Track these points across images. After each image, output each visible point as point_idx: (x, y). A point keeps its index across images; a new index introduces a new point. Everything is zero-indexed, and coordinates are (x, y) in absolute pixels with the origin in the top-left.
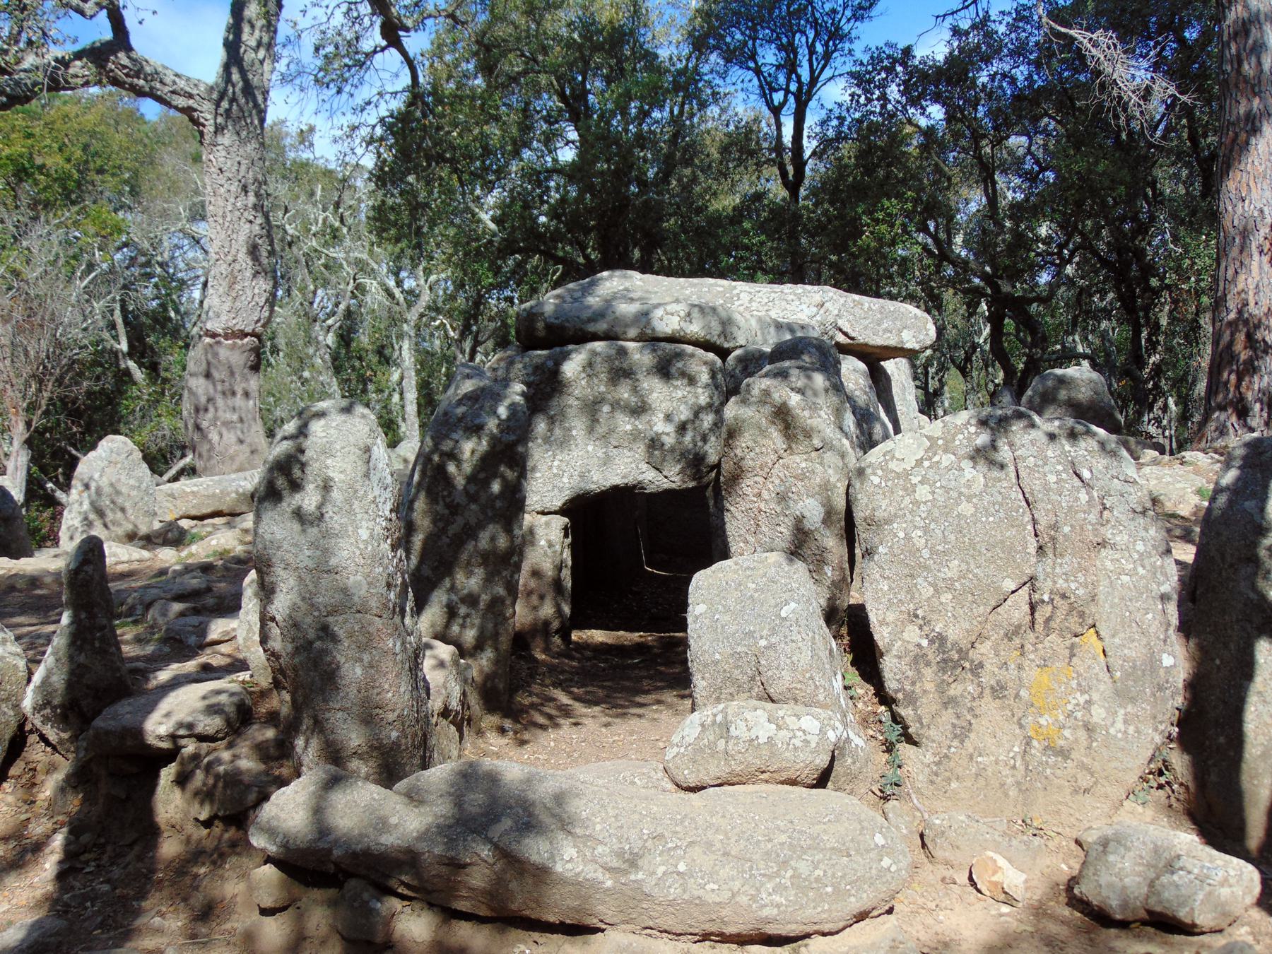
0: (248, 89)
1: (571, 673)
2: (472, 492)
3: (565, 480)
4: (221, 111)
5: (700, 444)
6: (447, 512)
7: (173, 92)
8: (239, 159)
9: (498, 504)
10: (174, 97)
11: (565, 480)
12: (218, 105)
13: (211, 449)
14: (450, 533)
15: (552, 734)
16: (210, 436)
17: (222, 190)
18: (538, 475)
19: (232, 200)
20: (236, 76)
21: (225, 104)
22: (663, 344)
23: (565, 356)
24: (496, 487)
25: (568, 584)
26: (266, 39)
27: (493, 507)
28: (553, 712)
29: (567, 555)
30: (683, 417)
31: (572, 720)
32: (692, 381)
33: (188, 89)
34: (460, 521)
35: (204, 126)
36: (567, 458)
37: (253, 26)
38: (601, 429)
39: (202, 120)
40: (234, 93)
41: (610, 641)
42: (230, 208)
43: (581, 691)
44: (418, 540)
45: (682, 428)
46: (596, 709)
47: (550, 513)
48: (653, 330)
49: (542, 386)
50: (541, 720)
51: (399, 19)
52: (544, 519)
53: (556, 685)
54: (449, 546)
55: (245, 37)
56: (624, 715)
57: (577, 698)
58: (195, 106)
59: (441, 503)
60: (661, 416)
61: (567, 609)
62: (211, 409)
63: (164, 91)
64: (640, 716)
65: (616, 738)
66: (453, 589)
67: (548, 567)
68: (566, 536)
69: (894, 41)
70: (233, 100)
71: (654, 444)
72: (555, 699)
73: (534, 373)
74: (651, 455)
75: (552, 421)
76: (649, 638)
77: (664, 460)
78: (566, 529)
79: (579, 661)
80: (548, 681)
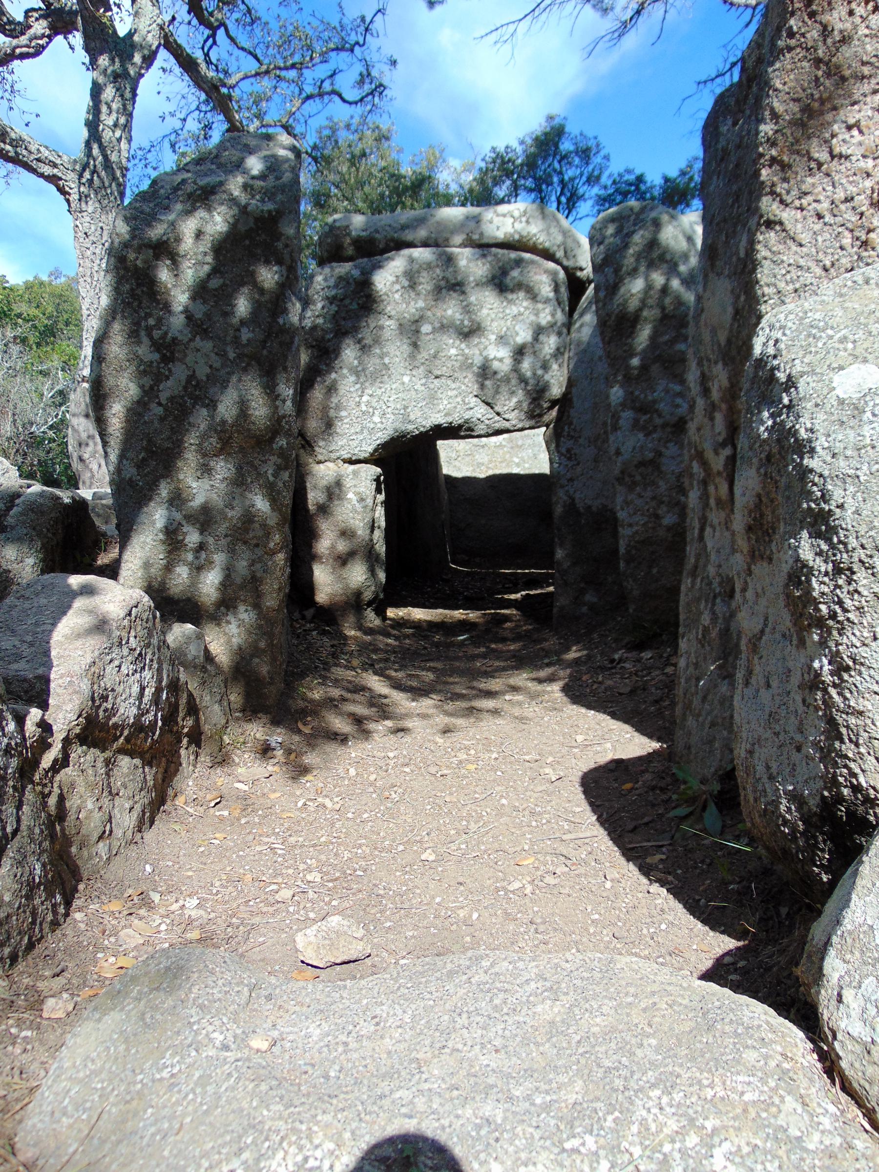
0: (107, 164)
1: (386, 652)
2: (199, 315)
3: (376, 419)
4: (84, 180)
5: (540, 372)
6: (156, 356)
7: (38, 160)
8: (101, 224)
9: (246, 335)
10: (40, 165)
11: (376, 419)
12: (81, 176)
13: (93, 476)
14: (164, 397)
15: (355, 750)
16: (91, 466)
17: (89, 253)
18: (343, 413)
19: (98, 262)
20: (96, 151)
21: (87, 175)
22: (494, 250)
23: (378, 266)
24: (242, 306)
25: (381, 548)
26: (122, 120)
27: (236, 340)
28: (360, 710)
29: (380, 513)
30: (520, 340)
31: (389, 723)
32: (533, 295)
33: (52, 159)
34: (180, 372)
35: (69, 194)
36: (379, 392)
37: (109, 107)
38: (424, 355)
39: (67, 189)
40: (95, 166)
41: (429, 618)
42: (96, 268)
43: (400, 675)
44: (116, 412)
45: (519, 352)
46: (426, 704)
47: (358, 462)
48: (481, 234)
49: (347, 301)
50: (339, 724)
51: (241, 123)
52: (352, 467)
53: (369, 666)
54: (162, 419)
55: (103, 117)
56: (471, 711)
57: (397, 686)
58: (60, 174)
59: (145, 340)
60: (493, 337)
61: (382, 576)
62: (91, 443)
63: (31, 159)
64: (495, 712)
65: (463, 756)
66: (177, 500)
67: (360, 526)
68: (378, 490)
69: (631, 167)
70: (94, 172)
71: (485, 372)
72: (364, 689)
73: (336, 286)
74: (482, 386)
75: (365, 349)
76: (473, 615)
77: (497, 392)
78: (377, 480)
79: (397, 638)
80: (355, 662)
